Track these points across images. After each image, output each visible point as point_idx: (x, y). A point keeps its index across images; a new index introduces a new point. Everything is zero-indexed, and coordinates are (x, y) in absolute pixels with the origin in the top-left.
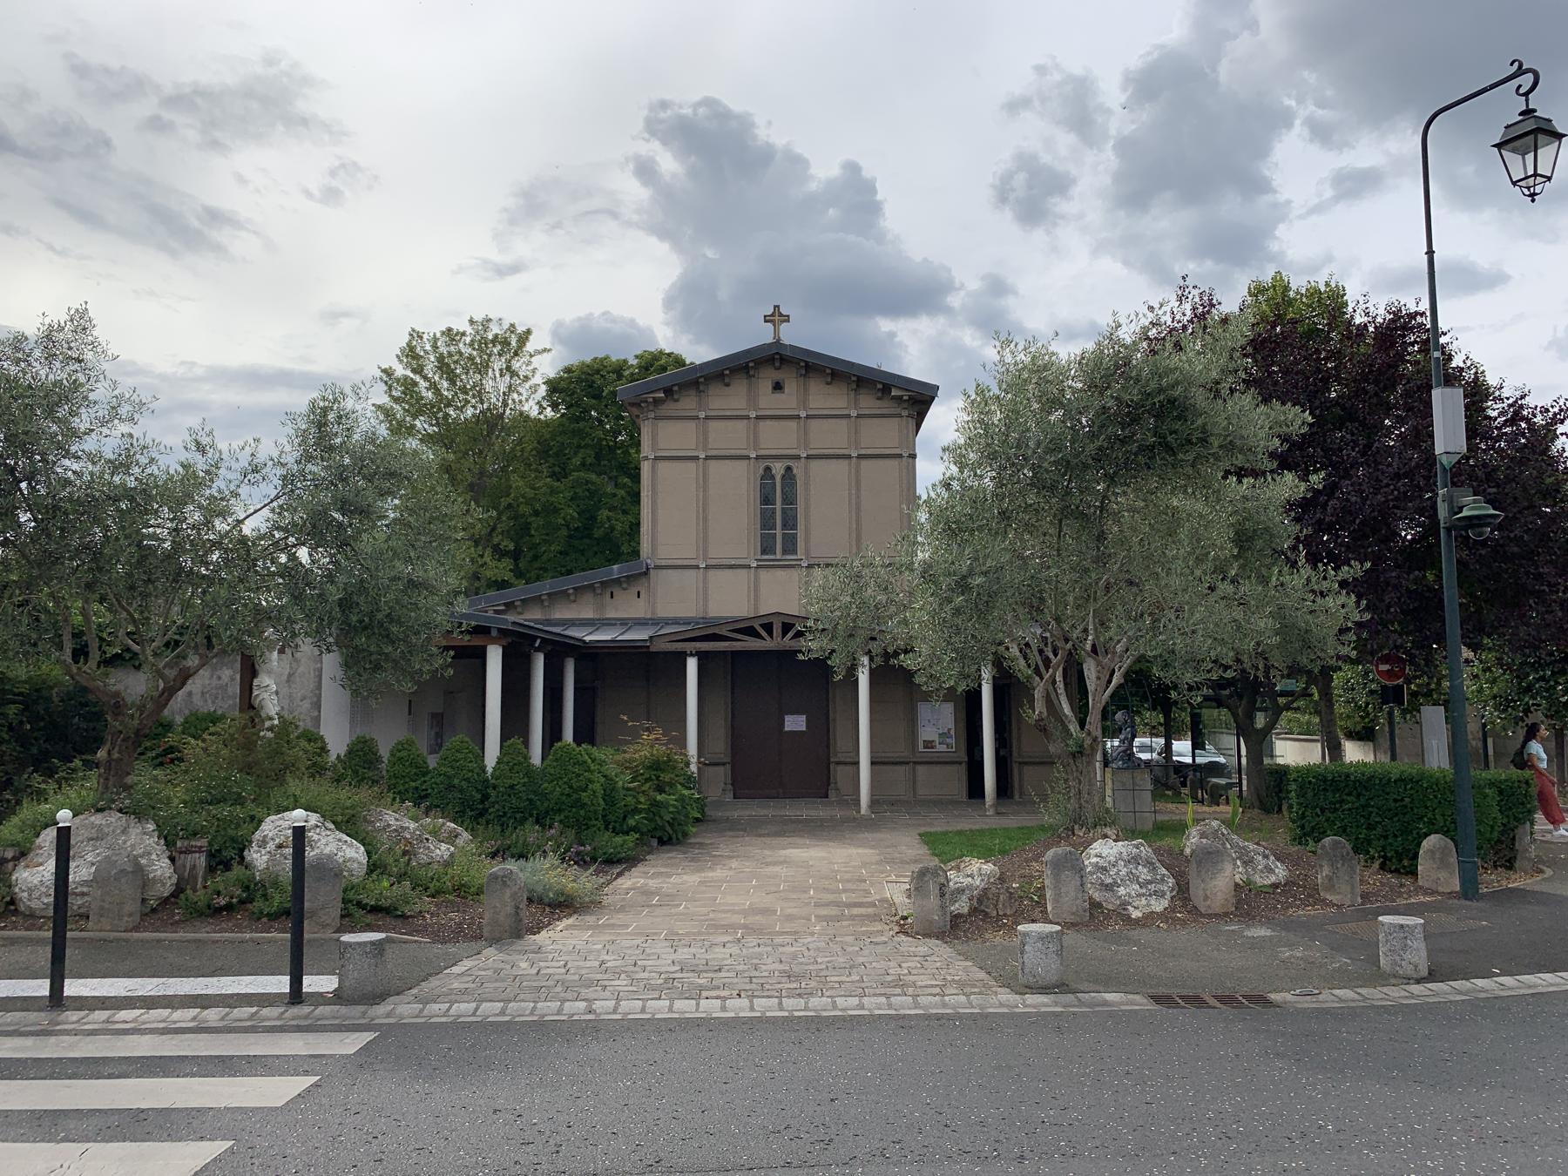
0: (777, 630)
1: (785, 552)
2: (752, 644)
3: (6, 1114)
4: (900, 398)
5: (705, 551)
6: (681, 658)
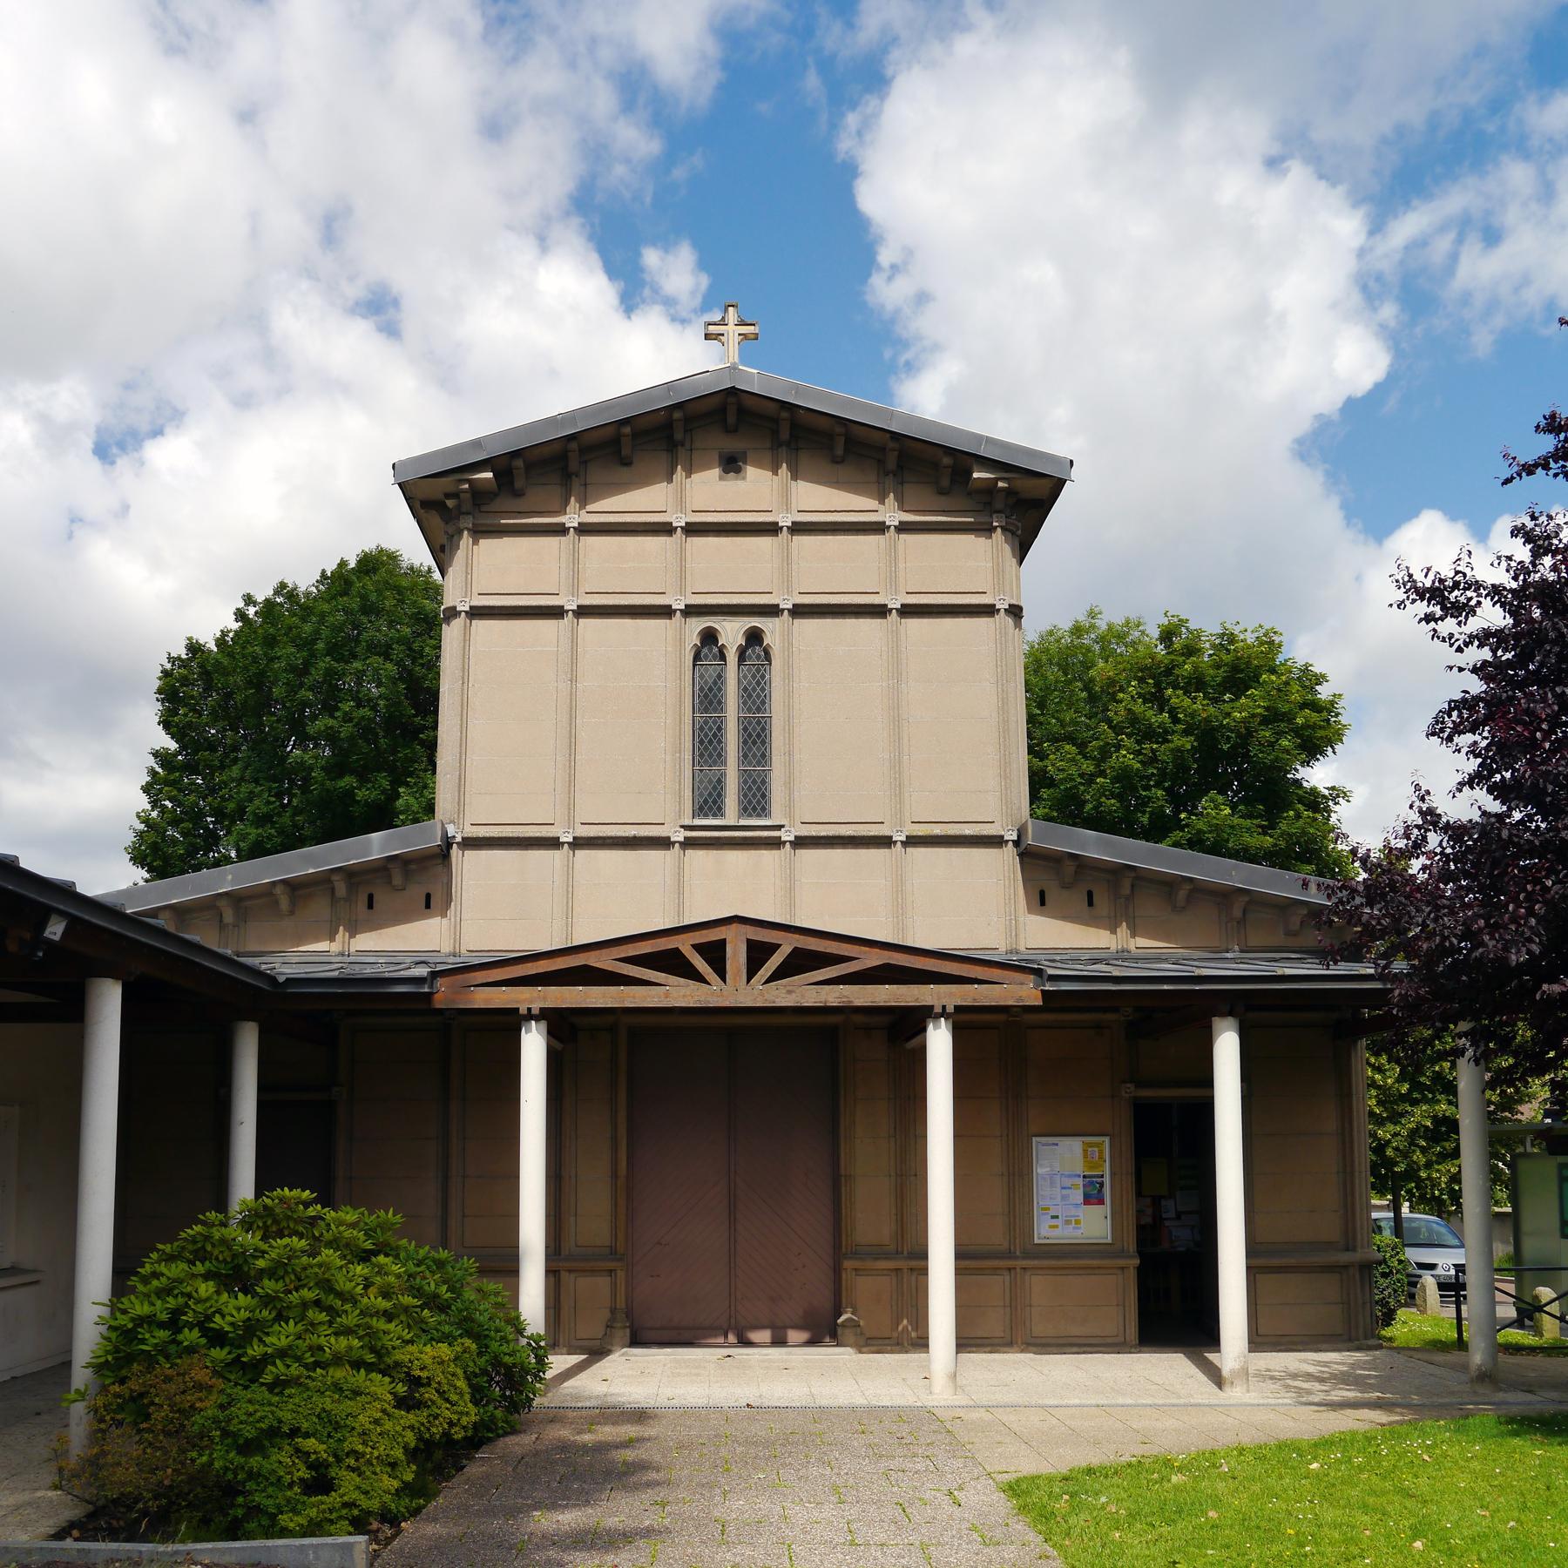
0: (737, 956)
1: (747, 808)
2: (676, 993)
3: (1566, 1355)
4: (989, 489)
5: (571, 807)
6: (508, 1024)
